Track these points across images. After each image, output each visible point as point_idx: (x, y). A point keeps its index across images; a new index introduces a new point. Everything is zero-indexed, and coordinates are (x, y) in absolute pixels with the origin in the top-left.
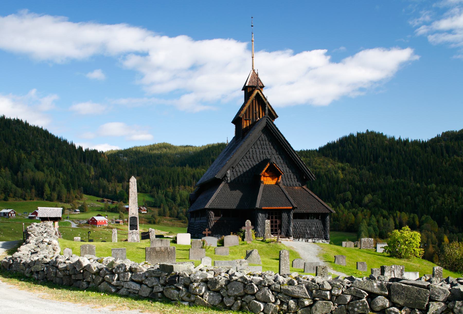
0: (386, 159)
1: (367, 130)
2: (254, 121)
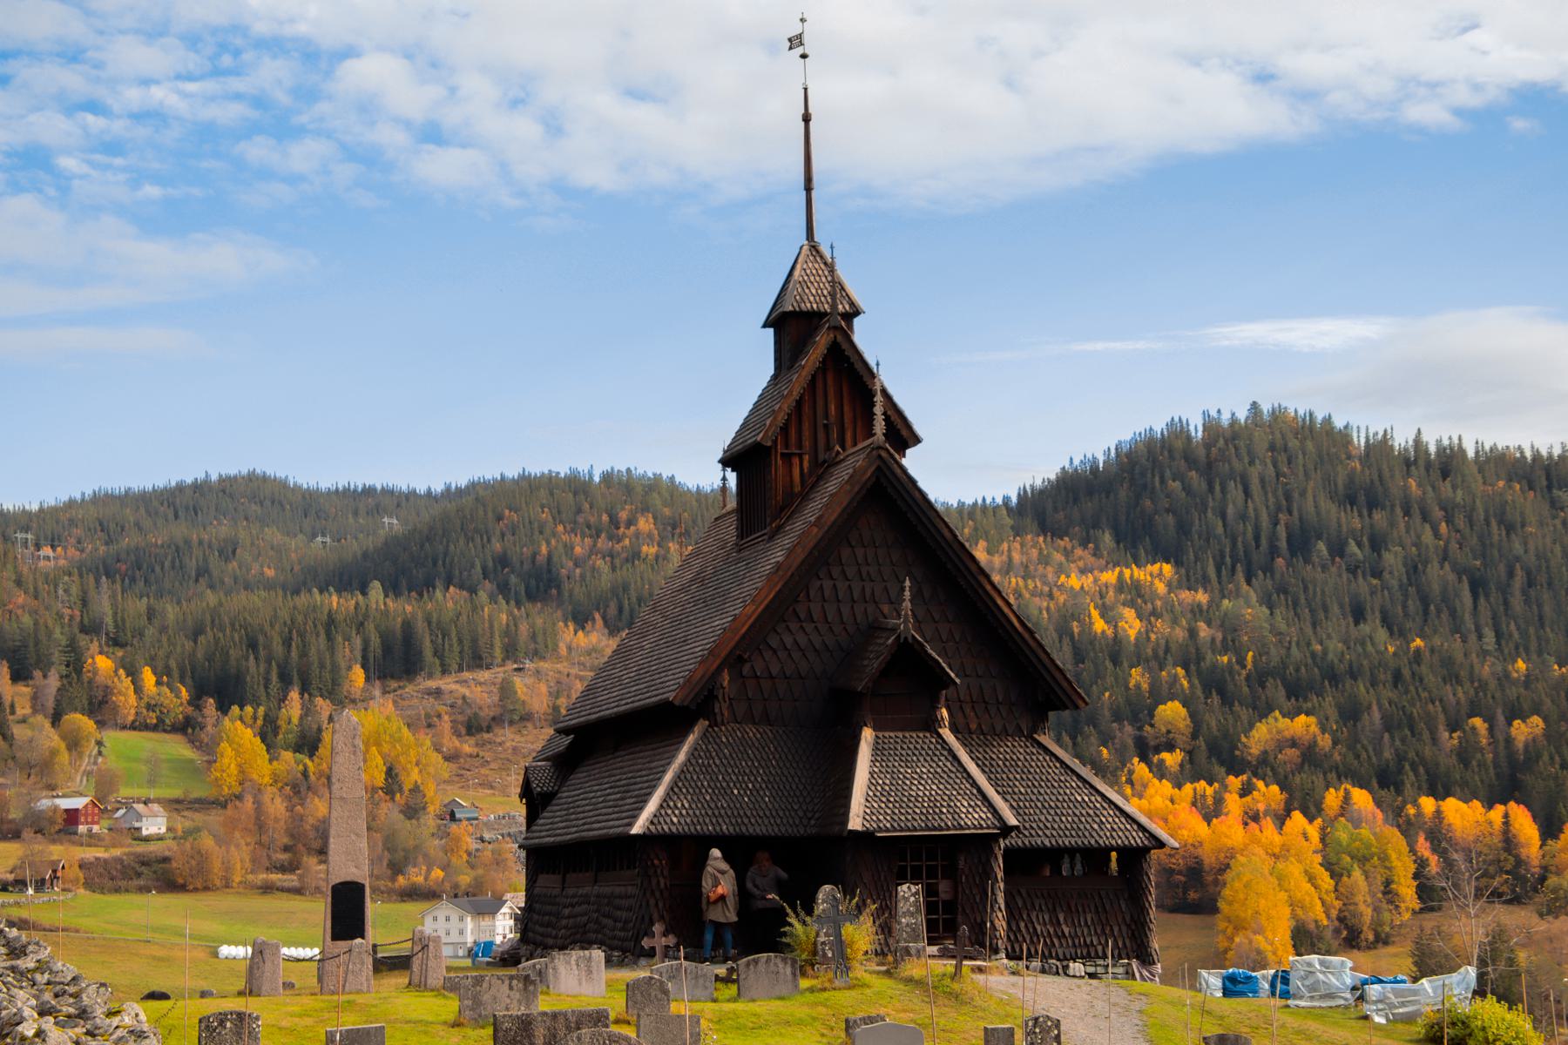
0: (1353, 547)
1: (1254, 405)
2: (821, 457)
